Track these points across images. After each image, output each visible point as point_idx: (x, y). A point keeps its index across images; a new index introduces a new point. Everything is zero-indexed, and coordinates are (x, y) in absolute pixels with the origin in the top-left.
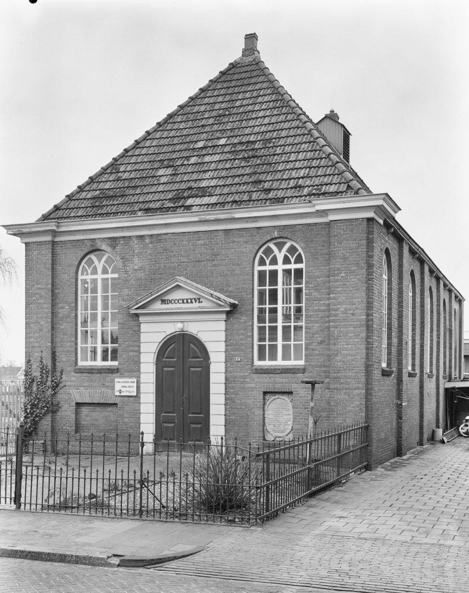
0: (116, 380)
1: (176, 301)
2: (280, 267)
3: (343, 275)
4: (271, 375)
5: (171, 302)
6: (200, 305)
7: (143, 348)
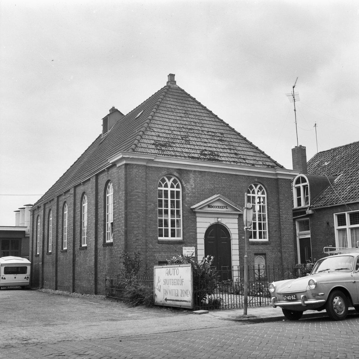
0: (184, 248)
1: (216, 207)
2: (169, 189)
3: (284, 202)
4: (257, 246)
5: (213, 207)
6: (227, 210)
7: (198, 230)
